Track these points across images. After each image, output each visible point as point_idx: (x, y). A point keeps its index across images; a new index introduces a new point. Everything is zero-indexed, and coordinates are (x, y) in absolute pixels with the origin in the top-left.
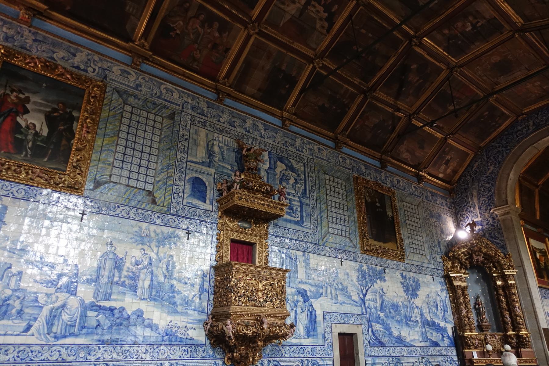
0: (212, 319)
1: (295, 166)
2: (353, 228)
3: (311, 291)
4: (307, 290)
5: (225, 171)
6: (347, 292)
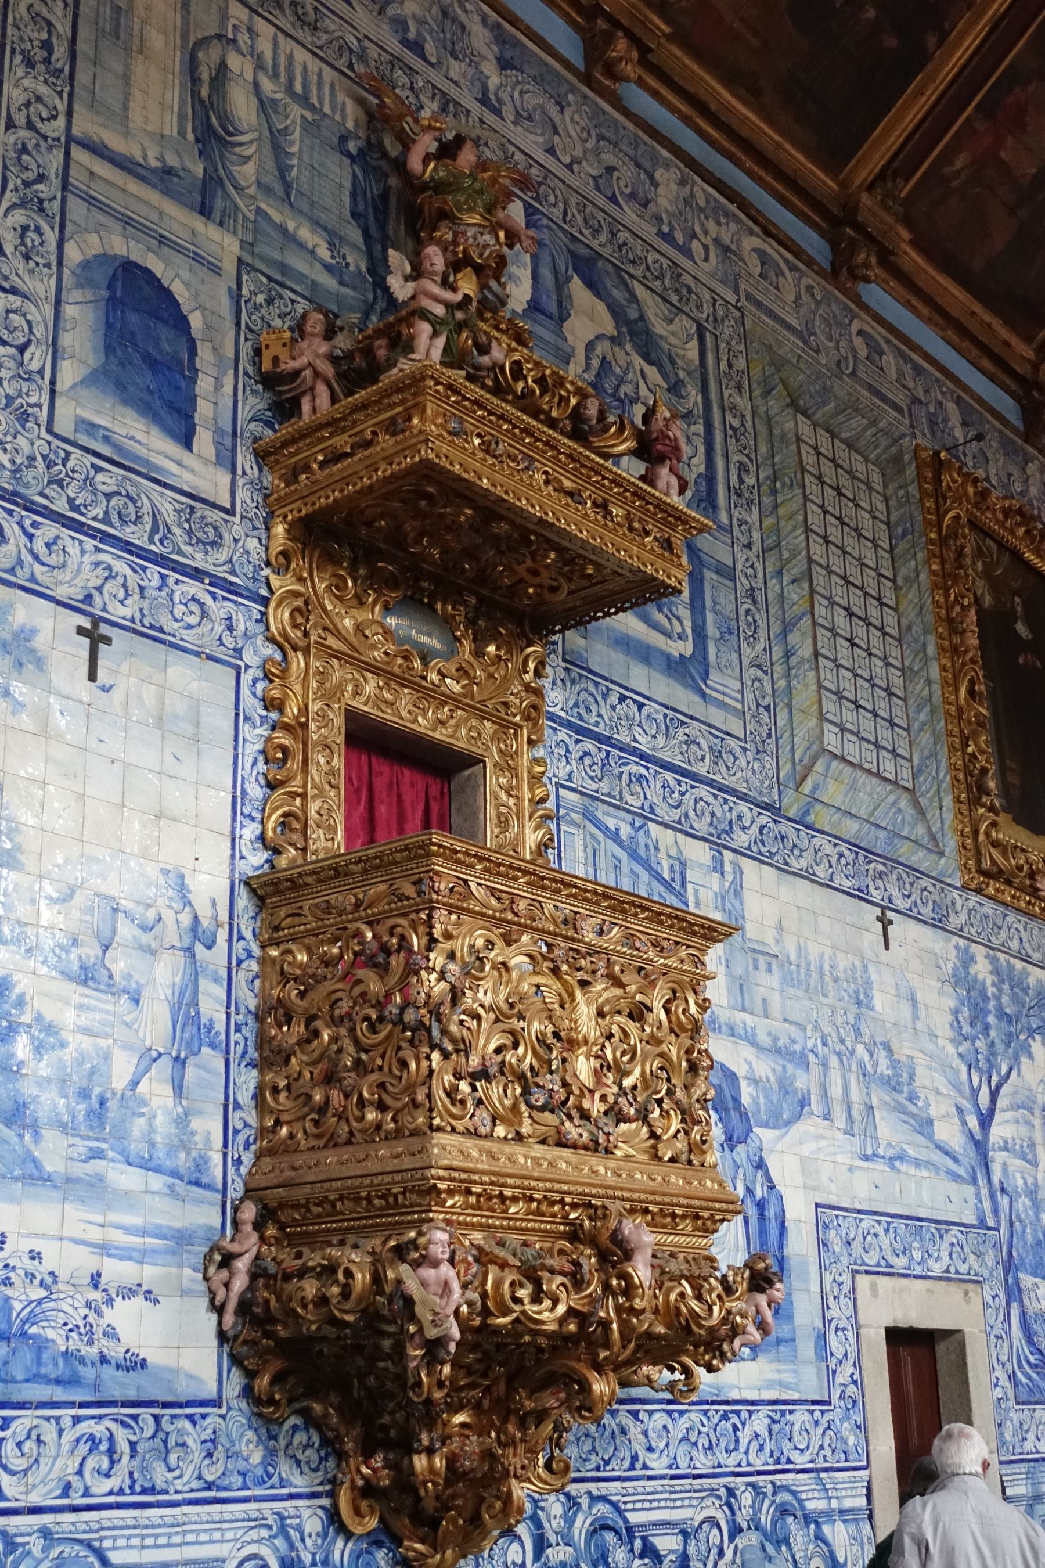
0: (258, 1226)
1: (659, 328)
2: (925, 739)
3: (755, 1081)
4: (741, 1071)
5: (298, 263)
6: (912, 1098)
